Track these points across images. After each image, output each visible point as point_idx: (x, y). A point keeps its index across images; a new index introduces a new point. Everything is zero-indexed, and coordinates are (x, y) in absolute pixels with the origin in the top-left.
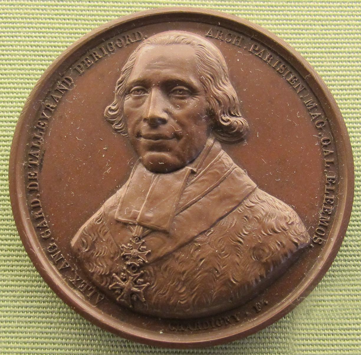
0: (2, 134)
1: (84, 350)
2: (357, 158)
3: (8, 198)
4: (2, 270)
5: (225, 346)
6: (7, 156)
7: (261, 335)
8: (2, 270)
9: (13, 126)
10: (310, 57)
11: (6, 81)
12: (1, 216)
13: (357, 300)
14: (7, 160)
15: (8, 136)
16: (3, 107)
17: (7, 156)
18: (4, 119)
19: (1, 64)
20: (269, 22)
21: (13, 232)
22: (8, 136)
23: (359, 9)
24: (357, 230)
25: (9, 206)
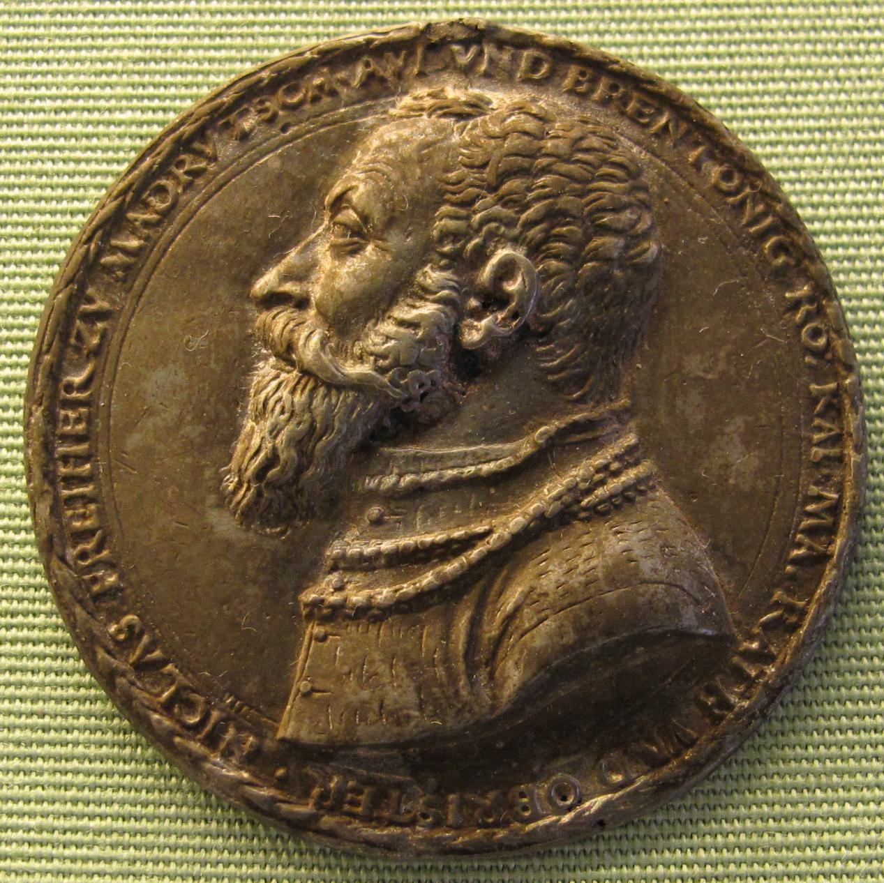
0: (6, 750)
1: (221, 865)
2: (873, 505)
3: (23, 524)
4: (5, 671)
5: (607, 847)
6: (16, 409)
7: (660, 817)
8: (5, 671)
9: (21, 379)
10: (764, 145)
11: (19, 55)
12: (2, 177)
13: (876, 154)
14: (18, 421)
15: (22, 340)
16: (8, 25)
17: (16, 409)
18: (9, 564)
19: (3, 599)
20: (795, 136)
21: (60, 634)
22: (22, 340)
23: (879, 238)
24: (873, 324)
25: (24, 506)
